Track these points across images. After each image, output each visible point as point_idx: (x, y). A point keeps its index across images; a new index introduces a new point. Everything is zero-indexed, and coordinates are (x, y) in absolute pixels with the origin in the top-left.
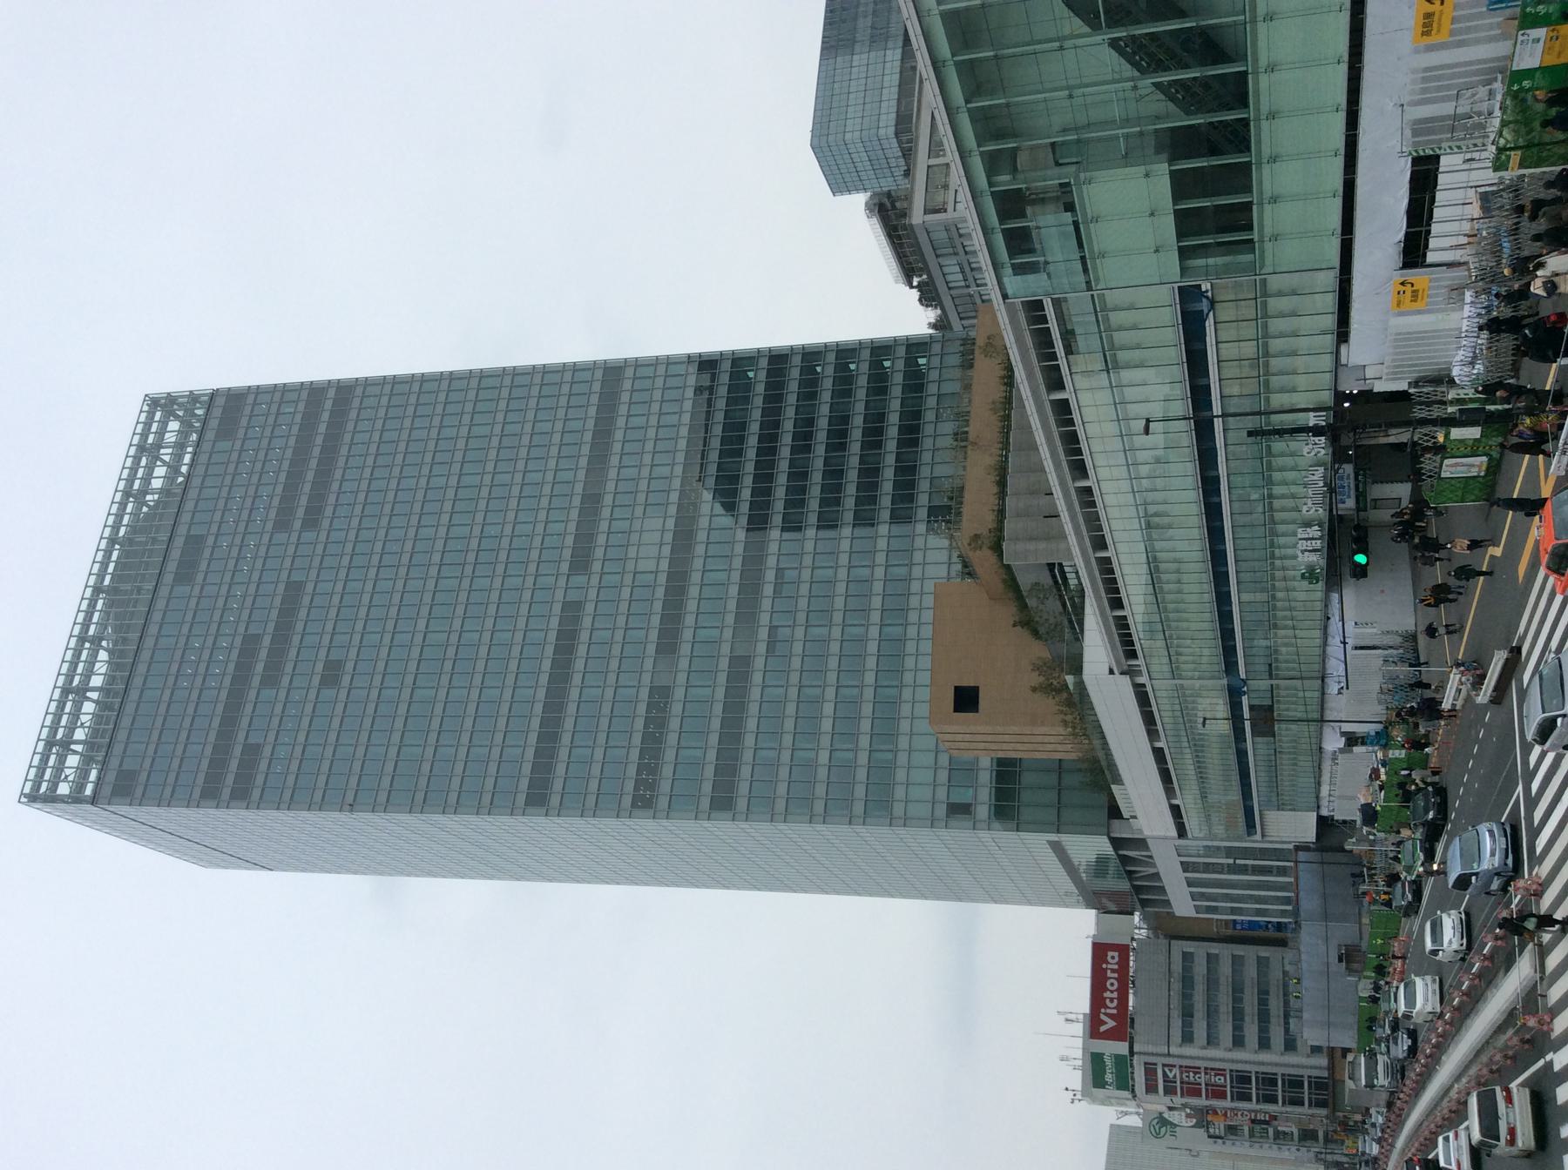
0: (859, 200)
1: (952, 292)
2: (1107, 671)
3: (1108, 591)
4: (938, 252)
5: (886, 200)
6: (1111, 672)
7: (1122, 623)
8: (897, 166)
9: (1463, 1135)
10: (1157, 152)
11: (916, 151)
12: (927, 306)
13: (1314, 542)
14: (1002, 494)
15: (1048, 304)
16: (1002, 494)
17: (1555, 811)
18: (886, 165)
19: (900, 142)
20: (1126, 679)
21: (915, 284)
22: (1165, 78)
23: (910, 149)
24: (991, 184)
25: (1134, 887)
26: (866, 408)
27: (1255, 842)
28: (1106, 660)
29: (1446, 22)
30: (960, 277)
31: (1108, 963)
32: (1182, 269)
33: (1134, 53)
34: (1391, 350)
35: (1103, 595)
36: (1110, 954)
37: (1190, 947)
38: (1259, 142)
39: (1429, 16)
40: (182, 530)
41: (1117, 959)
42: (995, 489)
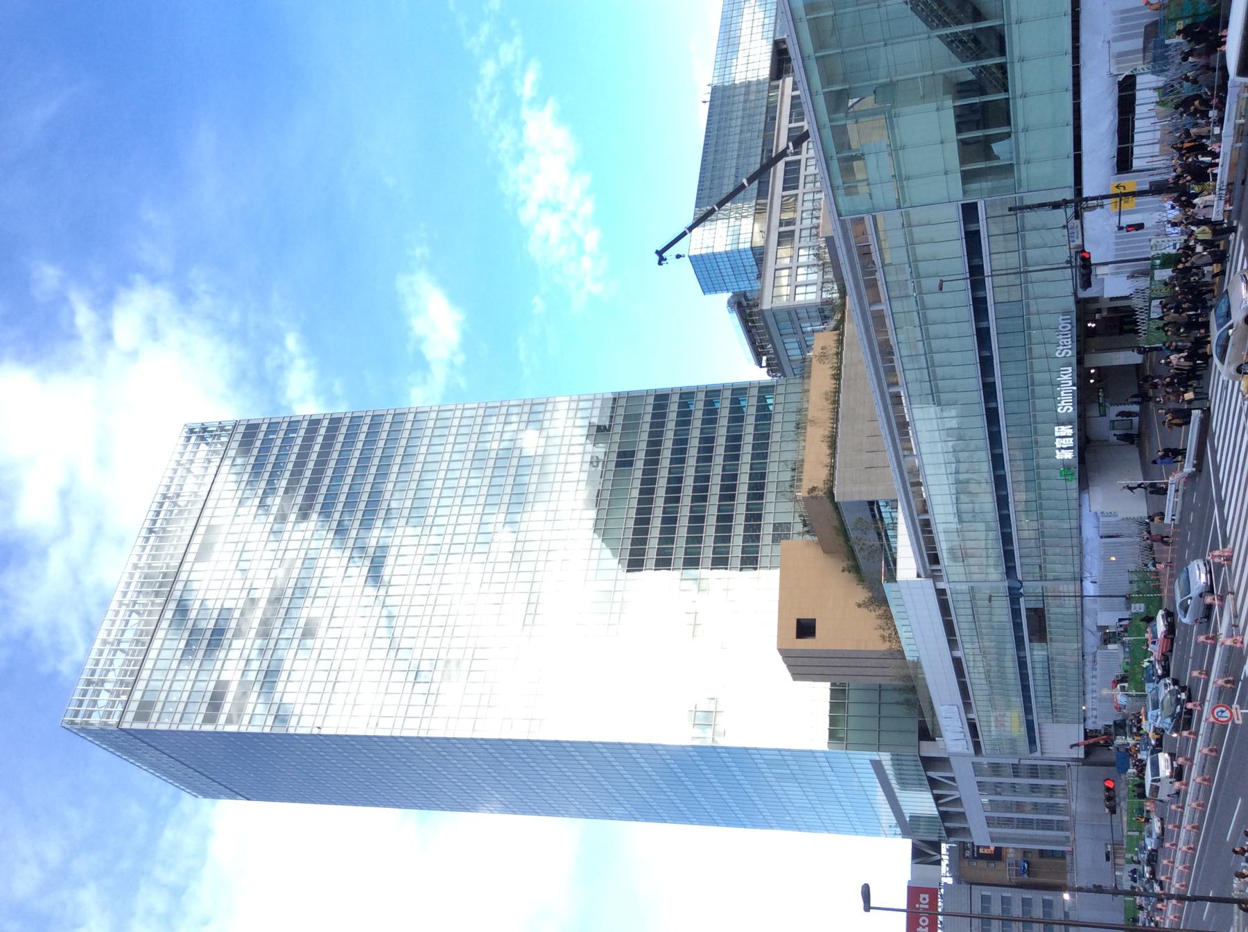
4: (782, 332)
6: (919, 576)
7: (926, 525)
8: (752, 272)
10: (944, 94)
11: (766, 259)
13: (1067, 439)
14: (833, 455)
16: (833, 455)
18: (744, 272)
21: (764, 364)
22: (948, 31)
23: (762, 260)
24: (831, 120)
25: (941, 813)
27: (1036, 759)
28: (915, 567)
30: (798, 352)
31: (920, 903)
33: (928, 16)
34: (1114, 247)
36: (922, 896)
37: (986, 891)
40: (204, 521)
41: (927, 901)
42: (828, 452)
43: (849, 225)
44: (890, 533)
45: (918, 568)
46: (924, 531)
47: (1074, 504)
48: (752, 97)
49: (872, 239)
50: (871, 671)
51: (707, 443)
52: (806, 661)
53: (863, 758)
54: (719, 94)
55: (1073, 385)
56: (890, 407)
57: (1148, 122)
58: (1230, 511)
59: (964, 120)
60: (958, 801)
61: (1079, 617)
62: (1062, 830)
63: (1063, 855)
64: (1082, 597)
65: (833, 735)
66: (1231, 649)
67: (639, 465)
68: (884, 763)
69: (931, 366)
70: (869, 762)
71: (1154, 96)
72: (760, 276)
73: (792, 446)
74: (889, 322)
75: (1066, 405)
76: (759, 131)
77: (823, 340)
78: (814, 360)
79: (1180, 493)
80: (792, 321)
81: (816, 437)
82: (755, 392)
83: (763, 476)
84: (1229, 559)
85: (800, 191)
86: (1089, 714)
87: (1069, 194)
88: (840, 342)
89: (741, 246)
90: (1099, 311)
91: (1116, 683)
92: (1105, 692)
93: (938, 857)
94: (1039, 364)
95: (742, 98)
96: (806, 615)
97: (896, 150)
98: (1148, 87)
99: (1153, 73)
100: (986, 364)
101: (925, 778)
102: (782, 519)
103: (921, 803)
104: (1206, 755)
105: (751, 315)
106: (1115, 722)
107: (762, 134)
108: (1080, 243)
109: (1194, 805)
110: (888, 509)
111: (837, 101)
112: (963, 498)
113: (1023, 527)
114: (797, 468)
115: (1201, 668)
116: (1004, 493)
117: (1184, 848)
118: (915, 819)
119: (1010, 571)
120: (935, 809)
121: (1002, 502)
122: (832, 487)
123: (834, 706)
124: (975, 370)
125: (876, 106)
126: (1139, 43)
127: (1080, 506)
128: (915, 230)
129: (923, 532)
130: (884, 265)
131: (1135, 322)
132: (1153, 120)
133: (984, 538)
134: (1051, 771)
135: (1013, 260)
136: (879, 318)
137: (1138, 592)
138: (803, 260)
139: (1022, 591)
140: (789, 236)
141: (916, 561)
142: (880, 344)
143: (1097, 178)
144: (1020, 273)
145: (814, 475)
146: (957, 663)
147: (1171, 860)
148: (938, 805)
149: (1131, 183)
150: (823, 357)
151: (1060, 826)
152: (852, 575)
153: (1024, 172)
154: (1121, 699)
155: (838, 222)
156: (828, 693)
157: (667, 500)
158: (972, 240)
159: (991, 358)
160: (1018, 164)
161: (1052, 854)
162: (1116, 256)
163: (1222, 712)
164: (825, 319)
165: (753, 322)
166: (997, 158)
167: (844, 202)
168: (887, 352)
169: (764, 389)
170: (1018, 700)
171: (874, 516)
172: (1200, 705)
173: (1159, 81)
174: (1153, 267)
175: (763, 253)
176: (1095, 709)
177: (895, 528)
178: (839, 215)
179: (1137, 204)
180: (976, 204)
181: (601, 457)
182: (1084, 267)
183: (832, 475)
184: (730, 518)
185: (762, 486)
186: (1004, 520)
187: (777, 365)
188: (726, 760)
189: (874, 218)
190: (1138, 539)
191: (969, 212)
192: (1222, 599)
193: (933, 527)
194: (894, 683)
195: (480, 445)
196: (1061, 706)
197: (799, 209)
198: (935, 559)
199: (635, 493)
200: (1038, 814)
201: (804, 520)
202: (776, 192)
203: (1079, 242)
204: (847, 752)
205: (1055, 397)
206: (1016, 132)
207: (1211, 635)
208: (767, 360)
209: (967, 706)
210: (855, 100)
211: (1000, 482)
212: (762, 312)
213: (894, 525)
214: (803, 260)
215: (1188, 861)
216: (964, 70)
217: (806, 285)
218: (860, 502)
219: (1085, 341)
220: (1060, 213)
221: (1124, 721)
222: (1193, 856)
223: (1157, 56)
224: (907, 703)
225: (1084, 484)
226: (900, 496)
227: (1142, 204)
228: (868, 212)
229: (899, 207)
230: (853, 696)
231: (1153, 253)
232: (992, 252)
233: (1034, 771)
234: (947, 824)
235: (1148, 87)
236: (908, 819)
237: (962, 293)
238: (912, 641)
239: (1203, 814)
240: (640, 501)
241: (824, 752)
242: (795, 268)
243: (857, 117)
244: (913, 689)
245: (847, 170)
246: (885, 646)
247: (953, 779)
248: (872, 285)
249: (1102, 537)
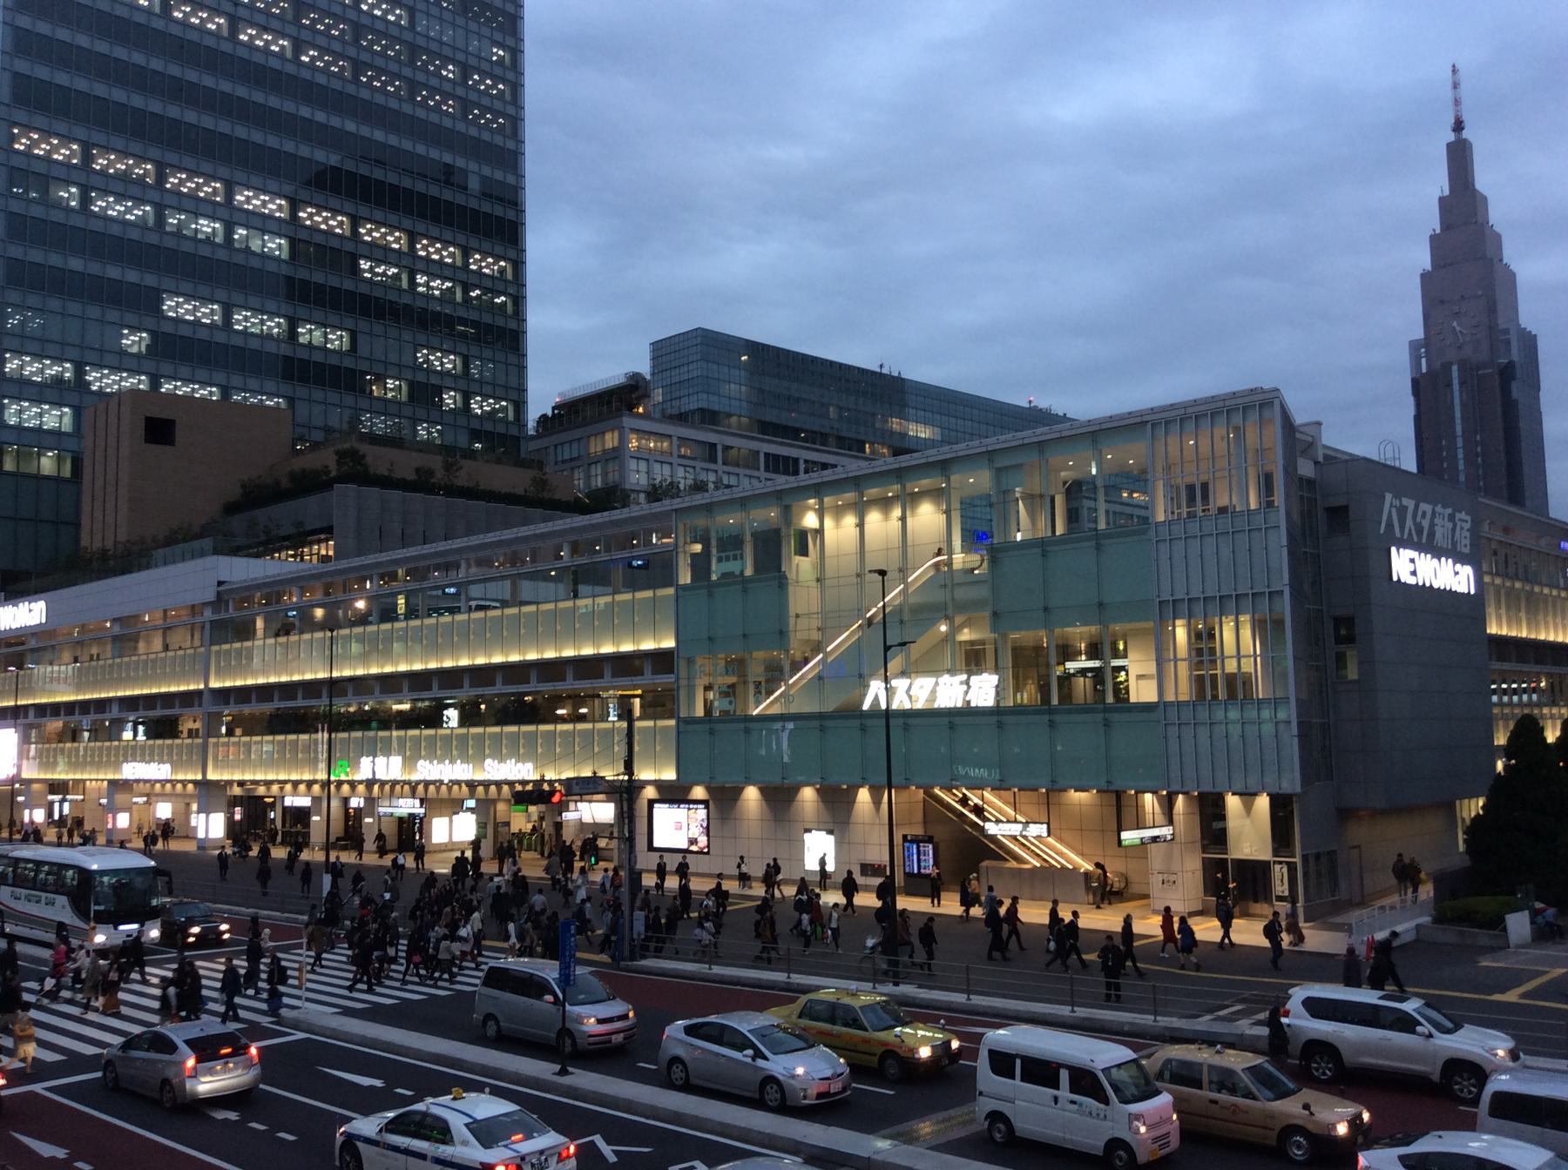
0: (644, 368)
1: (552, 448)
2: (222, 579)
6: (220, 583)
9: (215, 995)
12: (538, 422)
17: (68, 1039)
19: (693, 412)
20: (210, 596)
23: (686, 421)
30: (567, 456)
42: (235, 493)
85: (762, 474)
96: (180, 434)
140: (710, 455)
202: (804, 451)
217: (648, 473)
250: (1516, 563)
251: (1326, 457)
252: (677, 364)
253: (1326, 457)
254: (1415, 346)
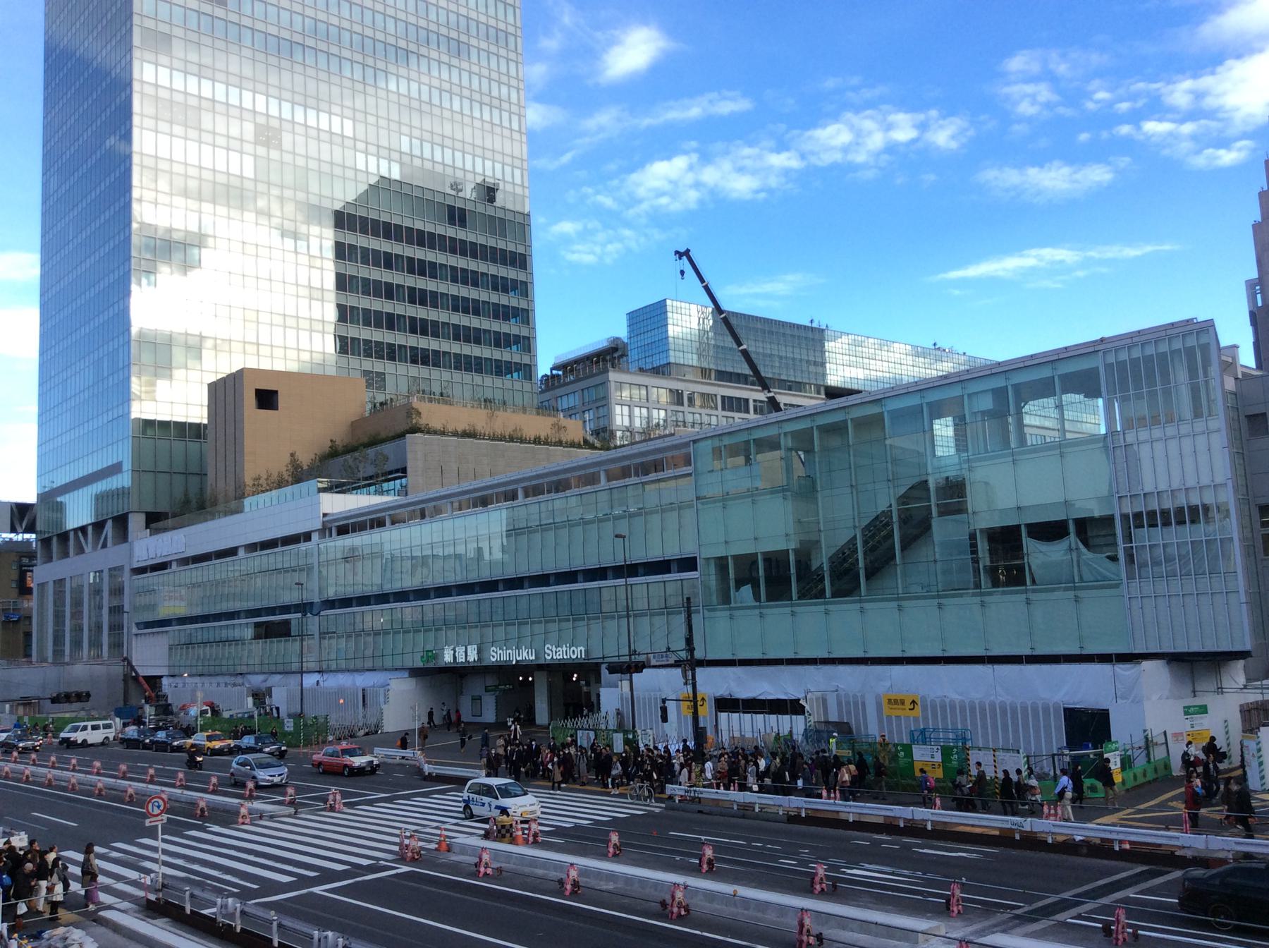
0: (622, 332)
3: (354, 525)
4: (586, 391)
5: (619, 353)
6: (325, 515)
7: (379, 523)
14: (455, 434)
15: (690, 469)
16: (455, 434)
21: (554, 372)
23: (658, 373)
26: (485, 331)
27: (130, 627)
28: (335, 511)
29: (899, 713)
30: (566, 406)
32: (708, 559)
33: (875, 526)
35: (496, 490)
38: (777, 606)
39: (903, 703)
42: (459, 430)
43: (684, 451)
44: (372, 488)
45: (333, 514)
46: (374, 521)
47: (398, 664)
48: (812, 368)
49: (670, 473)
50: (221, 466)
51: (474, 308)
52: (230, 399)
53: (123, 453)
54: (817, 337)
55: (517, 661)
56: (503, 489)
57: (761, 725)
58: (382, 808)
59: (775, 562)
60: (80, 550)
61: (280, 668)
62: (54, 654)
63: (28, 655)
64: (302, 672)
65: (148, 424)
66: (238, 813)
67: (452, 232)
68: (120, 476)
69: (543, 528)
70: (120, 459)
71: (785, 731)
72: (641, 370)
73: (468, 395)
74: (589, 488)
75: (497, 655)
76: (780, 374)
77: (575, 429)
78: (555, 419)
79: (404, 761)
80: (597, 400)
81: (478, 418)
82: (526, 360)
83: (437, 365)
84: (332, 809)
85: (720, 412)
86: (177, 680)
87: (699, 654)
88: (572, 445)
89: (672, 353)
90: (588, 684)
91: (212, 706)
92: (199, 695)
93: (19, 529)
94: (539, 628)
95: (812, 358)
97: (752, 495)
98: (794, 726)
99: (806, 730)
100: (542, 580)
101: (105, 517)
102: (390, 382)
103: (78, 513)
104: (126, 791)
105: (604, 360)
106: (170, 705)
107: (777, 377)
108: (652, 664)
109: (73, 781)
110: (398, 487)
111: (803, 441)
112: (408, 564)
113: (377, 617)
114: (444, 398)
115: (220, 785)
116: (411, 598)
117: (27, 772)
118: (60, 508)
119: (331, 604)
120: (71, 527)
121: (402, 596)
122: (422, 432)
123: (181, 427)
124: (536, 570)
125: (796, 478)
126: (833, 717)
127: (396, 669)
128: (676, 514)
129: (372, 520)
130: (643, 484)
131: (575, 716)
132: (762, 730)
133: (368, 579)
134: (117, 645)
135: (641, 604)
136: (592, 479)
137: (305, 725)
138: (655, 412)
139: (309, 615)
140: (678, 399)
141: (341, 513)
142: (567, 480)
143: (713, 683)
144: (628, 611)
145: (432, 414)
146: (232, 552)
147: (77, 768)
148: (75, 530)
149: (706, 712)
150: (559, 428)
151: (58, 653)
152: (327, 450)
153: (722, 615)
154: (194, 711)
155: (688, 440)
156: (197, 421)
157: (411, 260)
158: (662, 567)
159: (548, 585)
160: (731, 609)
161: (28, 645)
162: (638, 698)
163: (159, 807)
164: (596, 433)
165: (597, 362)
166: (738, 588)
167: (706, 446)
168: (560, 486)
169: (527, 370)
170: (198, 611)
171: (391, 472)
172: (182, 785)
173: (798, 736)
174: (626, 732)
175: (663, 374)
176: (184, 686)
177: (377, 493)
178: (695, 442)
179: (686, 717)
180: (696, 570)
181: (461, 194)
182: (630, 667)
183: (435, 433)
184: (391, 326)
185: (425, 363)
186: (383, 598)
187: (553, 385)
188: (116, 306)
189: (690, 475)
190: (361, 724)
191: (689, 564)
192: (292, 803)
193: (376, 530)
194: (209, 488)
195: (476, 50)
196: (187, 653)
197: (704, 411)
198: (343, 531)
199: (418, 225)
200: (71, 630)
201: (386, 403)
203: (653, 662)
204: (131, 438)
205: (506, 643)
206: (760, 607)
207: (255, 794)
208: (558, 375)
209: (185, 561)
210: (802, 456)
211: (422, 594)
212: (607, 371)
213: (381, 493)
214: (655, 412)
215: (58, 783)
216: (822, 559)
218: (405, 460)
219: (560, 670)
220: (682, 644)
221: (172, 713)
222: (19, 781)
223: (817, 734)
224: (187, 502)
225: (415, 673)
226: (411, 498)
227: (686, 724)
228: (695, 469)
229: (698, 498)
230: (194, 446)
231: (639, 732)
232: (650, 585)
233: (116, 628)
234: (55, 540)
235: (794, 726)
236: (59, 499)
237: (611, 555)
238: (254, 508)
239: (64, 789)
240: (410, 230)
241: (129, 413)
242: (647, 405)
243: (787, 461)
244: (202, 506)
245: (733, 451)
246: (248, 480)
247: (104, 546)
248: (625, 473)
249: (363, 690)
250: (226, 684)
251: (1244, 374)
252: (649, 328)
253: (1244, 374)
254: (1251, 285)
